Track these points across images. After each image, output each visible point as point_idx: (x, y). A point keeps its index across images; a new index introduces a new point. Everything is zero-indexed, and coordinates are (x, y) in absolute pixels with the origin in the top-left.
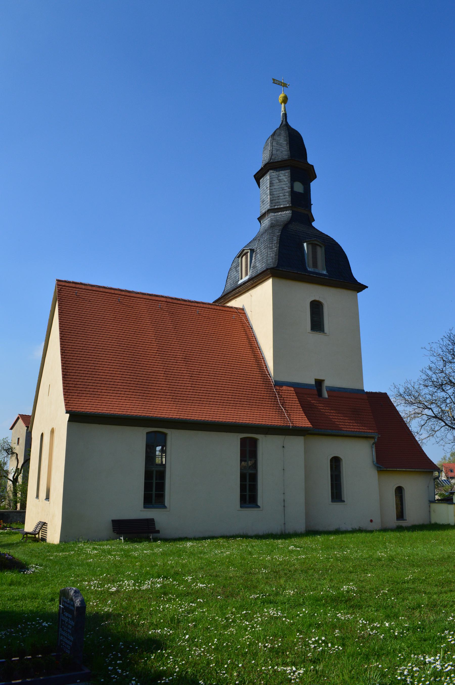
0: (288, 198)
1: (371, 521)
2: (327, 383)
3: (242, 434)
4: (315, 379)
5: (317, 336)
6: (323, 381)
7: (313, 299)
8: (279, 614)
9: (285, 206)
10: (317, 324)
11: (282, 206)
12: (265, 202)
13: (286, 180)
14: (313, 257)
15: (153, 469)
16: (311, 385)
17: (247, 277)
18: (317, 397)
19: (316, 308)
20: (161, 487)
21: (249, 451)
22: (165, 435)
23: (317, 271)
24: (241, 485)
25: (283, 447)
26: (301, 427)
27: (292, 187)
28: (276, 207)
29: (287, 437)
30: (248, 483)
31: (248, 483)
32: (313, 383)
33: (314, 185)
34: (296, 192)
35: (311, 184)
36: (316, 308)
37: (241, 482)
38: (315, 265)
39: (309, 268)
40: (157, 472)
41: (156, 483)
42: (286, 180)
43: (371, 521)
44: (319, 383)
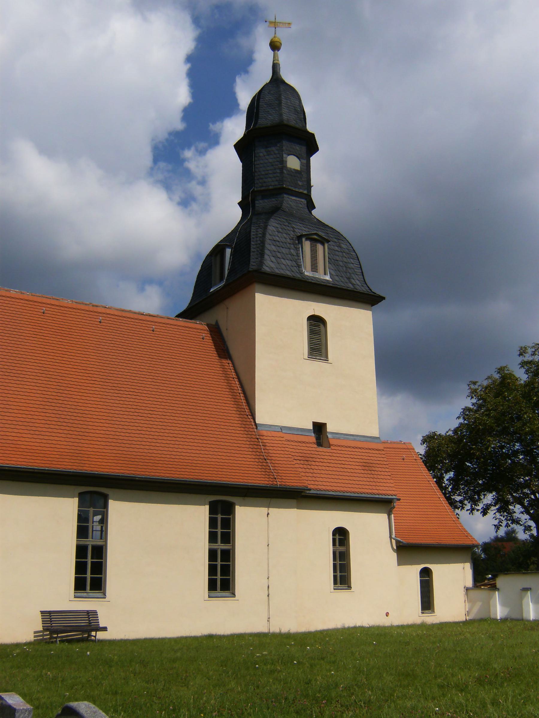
1: (387, 614)
3: (215, 496)
4: (313, 422)
5: (317, 365)
8: (522, 480)
9: (275, 187)
10: (318, 347)
11: (271, 187)
14: (312, 257)
15: (88, 543)
16: (308, 430)
18: (316, 446)
19: (316, 323)
20: (99, 568)
21: (222, 531)
23: (316, 275)
28: (263, 188)
32: (311, 427)
33: (314, 160)
34: (290, 168)
35: (311, 158)
36: (316, 323)
38: (314, 268)
40: (102, 577)
41: (92, 562)
43: (387, 614)
44: (319, 428)
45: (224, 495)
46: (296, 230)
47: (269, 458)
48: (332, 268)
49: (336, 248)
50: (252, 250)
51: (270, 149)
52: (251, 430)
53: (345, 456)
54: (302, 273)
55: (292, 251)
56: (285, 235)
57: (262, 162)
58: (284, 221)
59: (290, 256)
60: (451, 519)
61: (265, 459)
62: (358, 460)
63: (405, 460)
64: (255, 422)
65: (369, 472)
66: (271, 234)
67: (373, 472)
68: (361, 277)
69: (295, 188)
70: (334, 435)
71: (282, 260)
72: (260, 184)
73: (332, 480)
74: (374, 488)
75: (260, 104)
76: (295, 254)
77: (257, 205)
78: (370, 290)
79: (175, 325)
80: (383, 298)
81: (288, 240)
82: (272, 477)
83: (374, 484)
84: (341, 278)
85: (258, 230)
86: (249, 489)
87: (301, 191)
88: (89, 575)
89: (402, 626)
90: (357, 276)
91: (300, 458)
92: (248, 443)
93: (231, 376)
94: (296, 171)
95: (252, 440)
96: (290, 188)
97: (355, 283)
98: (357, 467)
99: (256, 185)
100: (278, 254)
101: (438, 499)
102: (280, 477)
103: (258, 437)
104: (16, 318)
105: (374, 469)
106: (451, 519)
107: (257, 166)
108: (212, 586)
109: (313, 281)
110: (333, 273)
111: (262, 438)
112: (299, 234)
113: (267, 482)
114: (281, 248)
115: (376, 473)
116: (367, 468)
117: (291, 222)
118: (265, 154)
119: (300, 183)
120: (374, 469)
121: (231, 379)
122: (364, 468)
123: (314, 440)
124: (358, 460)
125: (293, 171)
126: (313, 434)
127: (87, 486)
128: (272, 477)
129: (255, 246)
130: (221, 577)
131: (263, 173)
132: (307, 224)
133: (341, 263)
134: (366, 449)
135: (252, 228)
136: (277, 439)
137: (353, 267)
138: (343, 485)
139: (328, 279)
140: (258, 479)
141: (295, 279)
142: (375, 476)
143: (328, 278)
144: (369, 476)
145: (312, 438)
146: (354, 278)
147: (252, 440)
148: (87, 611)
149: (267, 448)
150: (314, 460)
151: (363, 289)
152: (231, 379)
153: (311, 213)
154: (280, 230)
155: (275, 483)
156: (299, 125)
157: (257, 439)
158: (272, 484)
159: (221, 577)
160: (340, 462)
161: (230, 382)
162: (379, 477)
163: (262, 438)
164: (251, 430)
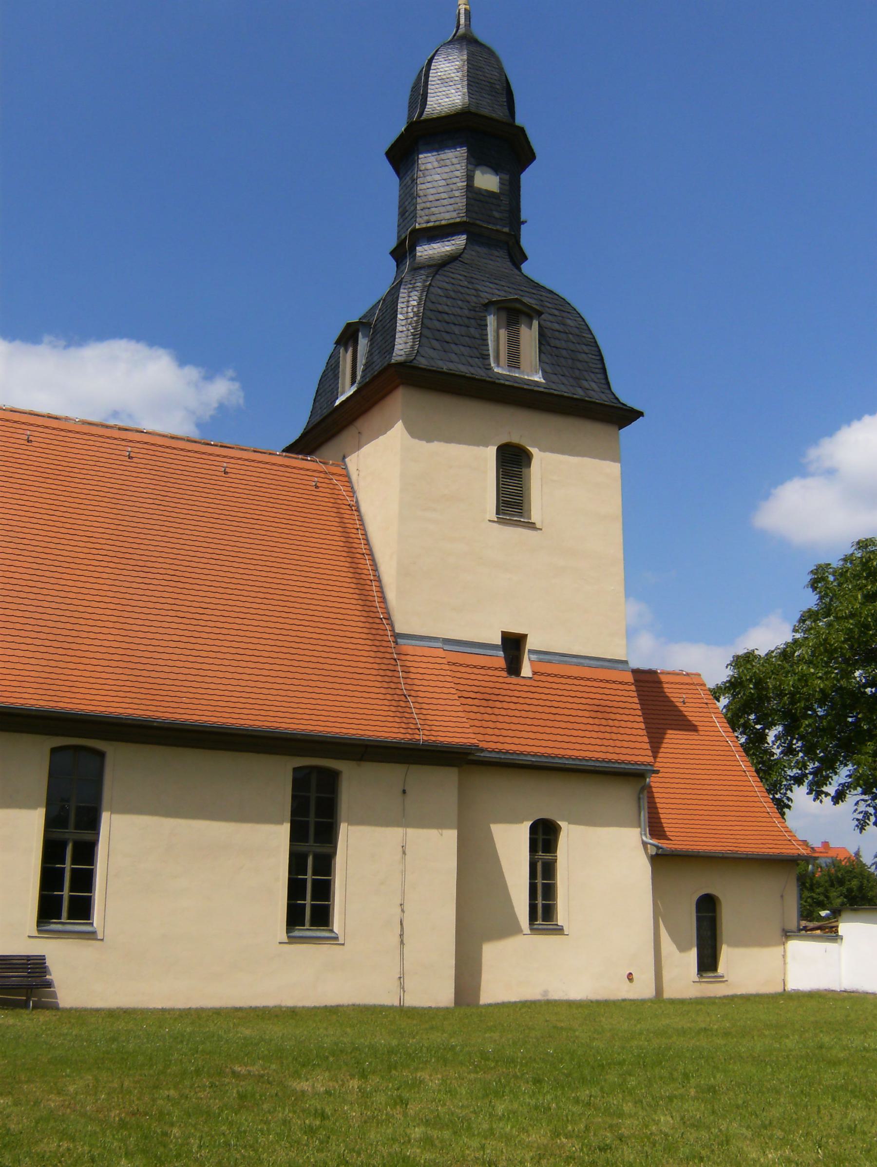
0: (462, 202)
1: (630, 977)
2: (531, 644)
3: (299, 759)
5: (514, 534)
6: (524, 637)
7: (504, 440)
12: (407, 214)
13: (455, 161)
15: (67, 836)
16: (493, 647)
17: (354, 389)
18: (504, 674)
22: (101, 755)
24: (530, 904)
25: (404, 792)
26: (449, 743)
27: (470, 178)
29: (414, 768)
30: (309, 877)
31: (309, 877)
32: (498, 641)
34: (480, 189)
35: (524, 177)
37: (697, 912)
38: (514, 360)
39: (498, 365)
42: (455, 161)
43: (630, 977)
44: (513, 644)
45: (321, 757)
46: (482, 294)
47: (413, 693)
48: (547, 361)
49: (556, 326)
50: (399, 328)
51: (443, 156)
52: (385, 644)
53: (560, 692)
54: (488, 368)
55: (472, 330)
56: (460, 303)
57: (429, 179)
58: (461, 278)
59: (467, 339)
60: (763, 810)
61: (405, 696)
62: (583, 701)
63: (687, 705)
64: (393, 630)
65: (604, 722)
66: (434, 300)
67: (611, 723)
68: (601, 376)
69: (489, 223)
70: (542, 657)
71: (453, 346)
72: (426, 218)
73: (573, 739)
74: (611, 749)
75: (430, 79)
76: (477, 336)
77: (418, 254)
78: (617, 399)
79: (287, 466)
80: (640, 414)
81: (466, 312)
82: (412, 726)
83: (611, 743)
84: (561, 377)
85: (412, 294)
86: (367, 746)
87: (499, 227)
88: (308, 902)
89: (606, 1001)
90: (592, 375)
91: (473, 695)
92: (376, 666)
93: (359, 551)
94: (491, 194)
95: (385, 661)
96: (478, 222)
97: (587, 387)
98: (580, 713)
99: (418, 220)
100: (444, 335)
101: (743, 773)
102: (428, 728)
103: (395, 656)
104: (130, 483)
105: (612, 716)
106: (763, 810)
107: (420, 187)
108: (294, 918)
109: (507, 383)
110: (548, 369)
111: (403, 657)
112: (487, 301)
113: (402, 736)
114: (452, 326)
115: (616, 723)
116: (600, 715)
117: (473, 281)
118: (436, 164)
119: (496, 214)
120: (612, 716)
121: (358, 556)
122: (593, 714)
123: (502, 663)
124: (583, 701)
125: (485, 194)
126: (501, 653)
127: (63, 735)
128: (412, 726)
129: (404, 323)
130: (309, 904)
131: (431, 198)
132: (503, 283)
133: (564, 353)
134: (601, 681)
135: (402, 290)
136: (430, 659)
137: (588, 360)
138: (578, 747)
139: (536, 379)
140: (384, 728)
141: (474, 379)
142: (614, 729)
143: (538, 378)
144: (602, 729)
145: (499, 659)
146: (588, 378)
147: (385, 661)
148: (28, 956)
149: (412, 676)
150: (501, 698)
151: (603, 398)
152: (358, 556)
153: (520, 270)
154: (452, 294)
155: (417, 737)
156: (500, 113)
157: (395, 659)
158: (411, 739)
159: (309, 904)
160: (549, 703)
161: (356, 560)
162: (622, 731)
163: (403, 657)
164: (385, 644)
